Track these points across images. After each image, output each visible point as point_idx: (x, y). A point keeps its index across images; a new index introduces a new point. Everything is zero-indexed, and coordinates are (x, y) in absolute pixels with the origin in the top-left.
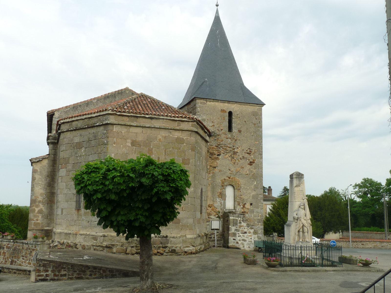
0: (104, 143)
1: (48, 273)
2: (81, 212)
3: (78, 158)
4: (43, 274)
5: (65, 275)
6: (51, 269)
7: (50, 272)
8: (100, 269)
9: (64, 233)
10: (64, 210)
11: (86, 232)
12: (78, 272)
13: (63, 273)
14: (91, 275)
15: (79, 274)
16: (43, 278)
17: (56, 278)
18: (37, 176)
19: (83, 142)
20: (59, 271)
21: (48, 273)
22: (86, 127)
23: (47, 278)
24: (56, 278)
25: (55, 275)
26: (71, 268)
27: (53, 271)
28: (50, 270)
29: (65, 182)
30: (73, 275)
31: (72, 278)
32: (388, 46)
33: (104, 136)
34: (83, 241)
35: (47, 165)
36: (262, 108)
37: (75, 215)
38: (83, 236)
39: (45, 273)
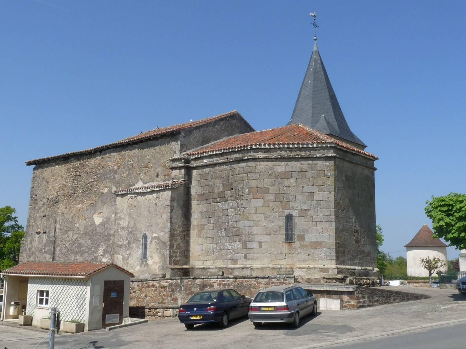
0: (327, 176)
1: (365, 300)
2: (296, 245)
3: (285, 189)
4: (361, 300)
5: (377, 301)
6: (367, 296)
7: (366, 299)
8: (400, 294)
9: (269, 268)
10: (263, 243)
11: (308, 265)
12: (386, 298)
13: (376, 299)
14: (394, 300)
15: (386, 299)
16: (361, 304)
17: (371, 304)
18: (175, 204)
19: (291, 172)
20: (373, 297)
21: (365, 300)
22: (300, 156)
23: (365, 304)
24: (371, 304)
25: (370, 301)
26: (380, 294)
27: (368, 298)
28: (366, 296)
29: (263, 212)
30: (382, 301)
31: (382, 303)
32: (292, 118)
33: (326, 168)
34: (305, 275)
35: (183, 193)
36: (374, 163)
37: (285, 248)
38: (305, 270)
39: (363, 300)
